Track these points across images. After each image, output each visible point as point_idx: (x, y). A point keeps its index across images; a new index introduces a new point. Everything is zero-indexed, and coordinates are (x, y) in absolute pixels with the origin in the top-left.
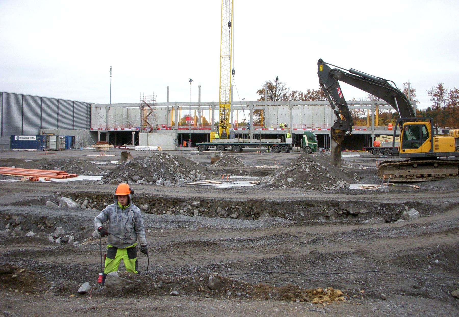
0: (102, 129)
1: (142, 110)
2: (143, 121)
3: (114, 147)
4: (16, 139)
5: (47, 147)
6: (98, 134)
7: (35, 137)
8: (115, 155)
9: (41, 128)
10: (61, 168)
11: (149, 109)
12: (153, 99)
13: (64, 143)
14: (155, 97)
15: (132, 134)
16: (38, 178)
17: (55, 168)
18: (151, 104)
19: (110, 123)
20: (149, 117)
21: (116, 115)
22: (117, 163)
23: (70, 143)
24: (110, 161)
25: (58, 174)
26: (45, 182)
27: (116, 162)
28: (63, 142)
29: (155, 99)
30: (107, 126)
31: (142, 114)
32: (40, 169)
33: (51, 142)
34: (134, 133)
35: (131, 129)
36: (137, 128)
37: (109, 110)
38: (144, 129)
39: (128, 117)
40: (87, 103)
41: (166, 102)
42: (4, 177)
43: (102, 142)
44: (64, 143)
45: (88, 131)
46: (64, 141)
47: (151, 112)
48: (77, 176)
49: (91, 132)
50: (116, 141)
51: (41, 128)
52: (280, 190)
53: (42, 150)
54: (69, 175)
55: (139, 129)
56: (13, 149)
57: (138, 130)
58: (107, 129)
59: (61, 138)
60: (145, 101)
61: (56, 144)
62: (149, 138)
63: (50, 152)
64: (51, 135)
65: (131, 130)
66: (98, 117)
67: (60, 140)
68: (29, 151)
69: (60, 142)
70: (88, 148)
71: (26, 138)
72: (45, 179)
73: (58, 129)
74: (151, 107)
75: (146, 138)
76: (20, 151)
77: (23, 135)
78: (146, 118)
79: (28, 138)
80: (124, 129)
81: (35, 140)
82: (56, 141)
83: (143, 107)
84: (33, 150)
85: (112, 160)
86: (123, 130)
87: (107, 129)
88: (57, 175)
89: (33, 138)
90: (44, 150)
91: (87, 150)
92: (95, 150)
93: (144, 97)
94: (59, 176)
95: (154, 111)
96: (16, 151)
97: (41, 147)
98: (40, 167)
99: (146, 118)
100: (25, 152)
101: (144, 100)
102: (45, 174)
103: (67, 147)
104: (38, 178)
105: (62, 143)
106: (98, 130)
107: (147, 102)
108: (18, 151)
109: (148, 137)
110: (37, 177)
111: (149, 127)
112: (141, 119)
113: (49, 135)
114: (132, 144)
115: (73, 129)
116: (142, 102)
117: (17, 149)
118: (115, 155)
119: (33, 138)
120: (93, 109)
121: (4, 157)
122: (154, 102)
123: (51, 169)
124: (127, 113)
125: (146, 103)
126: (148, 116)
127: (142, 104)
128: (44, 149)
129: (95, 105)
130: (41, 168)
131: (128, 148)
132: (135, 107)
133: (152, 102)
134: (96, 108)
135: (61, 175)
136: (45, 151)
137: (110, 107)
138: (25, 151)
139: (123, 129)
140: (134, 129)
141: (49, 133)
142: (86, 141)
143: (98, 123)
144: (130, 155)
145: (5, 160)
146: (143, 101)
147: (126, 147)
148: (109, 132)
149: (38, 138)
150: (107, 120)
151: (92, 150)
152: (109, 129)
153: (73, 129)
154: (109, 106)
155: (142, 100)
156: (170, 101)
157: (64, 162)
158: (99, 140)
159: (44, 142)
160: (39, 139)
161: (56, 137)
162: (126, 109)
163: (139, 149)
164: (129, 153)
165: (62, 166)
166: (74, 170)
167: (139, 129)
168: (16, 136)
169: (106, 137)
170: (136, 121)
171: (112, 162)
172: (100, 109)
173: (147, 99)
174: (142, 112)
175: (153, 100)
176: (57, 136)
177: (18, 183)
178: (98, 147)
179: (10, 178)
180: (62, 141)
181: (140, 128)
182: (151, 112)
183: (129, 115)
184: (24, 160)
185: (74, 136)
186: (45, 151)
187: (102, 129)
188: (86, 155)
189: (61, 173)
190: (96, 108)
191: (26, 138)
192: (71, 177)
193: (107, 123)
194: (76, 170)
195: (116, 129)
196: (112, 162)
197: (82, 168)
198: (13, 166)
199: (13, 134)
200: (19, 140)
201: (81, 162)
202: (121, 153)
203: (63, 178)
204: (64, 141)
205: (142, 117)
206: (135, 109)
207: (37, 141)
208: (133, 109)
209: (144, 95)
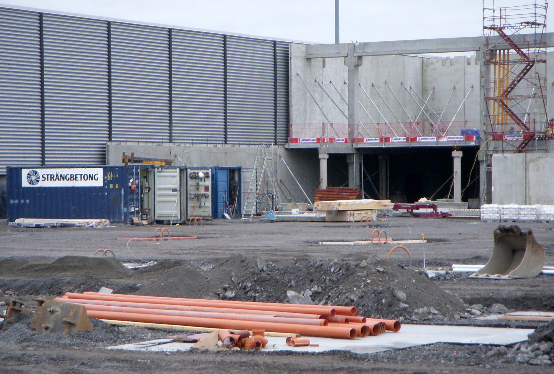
0: (332, 140)
1: (487, 63)
2: (495, 109)
3: (396, 208)
4: (25, 183)
5: (143, 212)
6: (318, 161)
7: (99, 172)
8: (429, 241)
9: (110, 139)
10: (309, 293)
11: (519, 57)
12: (532, 20)
13: (206, 196)
14: (541, 11)
15: (451, 159)
16: (262, 334)
17: (290, 293)
18: (526, 41)
19: (361, 118)
20: (513, 93)
21: (382, 85)
22: (481, 271)
23: (223, 196)
24: (446, 263)
25: (327, 318)
26: (289, 353)
27: (474, 268)
28: (202, 191)
29: (540, 20)
30: (351, 126)
31: (487, 81)
32: (224, 298)
33: (157, 192)
34: (457, 156)
35: (444, 140)
36: (467, 135)
37: (357, 66)
38: (498, 137)
39: (424, 91)
40: (275, 43)
41: (333, 42)
42: (112, 332)
43: (337, 189)
44: (206, 196)
45: (280, 150)
46: (207, 189)
47: (526, 71)
48: (396, 327)
49: (287, 149)
50: (383, 184)
51: (110, 139)
52: (149, 358)
53: (125, 222)
54: (371, 322)
55: (478, 138)
56: (18, 221)
57: (473, 144)
58: (353, 141)
59: (195, 177)
60: (500, 29)
61: (177, 199)
62: (532, 174)
63: (157, 229)
64: (157, 164)
65: (445, 141)
66: (317, 96)
67: (191, 182)
68: (80, 228)
69: (192, 190)
70: (295, 212)
71: (63, 178)
72: (288, 340)
73: (171, 141)
74: (524, 50)
75: (520, 173)
76: (44, 227)
77: (43, 165)
78: (507, 93)
79: (73, 178)
80: (418, 139)
81: (99, 183)
82: (177, 186)
83: (492, 53)
84: (93, 222)
85: (457, 261)
86: (413, 145)
87: (353, 141)
88: (325, 324)
89: (91, 177)
90: (132, 223)
91: (295, 220)
92: (323, 220)
93: (497, 13)
94: (331, 327)
95: (538, 67)
96: (28, 227)
97: (124, 210)
98: (225, 289)
99: (507, 93)
100: (65, 232)
101: (497, 23)
102: (271, 317)
103: (216, 214)
104: (262, 334)
105: (198, 197)
106: (317, 146)
107: (507, 32)
108: (38, 226)
109: (526, 169)
110: (259, 331)
111: (517, 127)
112: (487, 99)
113: (153, 167)
114: (451, 197)
115: (226, 143)
116: (487, 32)
117: (33, 222)
118: (429, 241)
119: (91, 177)
120: (296, 65)
121: (40, 254)
122: (539, 30)
123: (268, 299)
124: (419, 78)
125: (503, 35)
126: (513, 86)
127: (488, 39)
128: (136, 220)
129: (303, 48)
130: (230, 294)
131: (445, 210)
132: (452, 55)
133: (530, 30)
134: (309, 59)
135: (336, 322)
136: (138, 225)
137: (360, 57)
138: (64, 226)
139: (387, 140)
140: (458, 139)
141: (148, 160)
142: (275, 190)
143: (318, 120)
144: (534, 242)
145: (50, 262)
146: (493, 28)
147: (440, 210)
148: (358, 150)
149: (110, 176)
150: (351, 106)
151: (312, 220)
152: (361, 140)
153: (226, 143)
154: (359, 52)
155: (489, 24)
156: (341, 41)
157: (322, 269)
158: (324, 185)
159: (132, 192)
160: (114, 181)
161: (178, 170)
162: (418, 65)
163: (496, 216)
164: (530, 233)
165: (315, 288)
166: (369, 302)
167: (478, 138)
168: (25, 172)
169: (347, 171)
170: (456, 107)
171: (458, 268)
172: (324, 66)
173: (510, 21)
174: (488, 70)
175: (533, 24)
176: (183, 170)
177: (186, 358)
178: (336, 208)
179: (134, 337)
180: (198, 187)
181: (482, 135)
182: (526, 71)
183: (429, 86)
184: (118, 261)
185: (239, 169)
186: (138, 225)
187: (332, 140)
188: (317, 242)
189: (337, 317)
190: (309, 59)
191: (63, 178)
192: (377, 330)
193: (351, 116)
194: (379, 302)
195: (387, 140)
196: (458, 268)
197: (401, 295)
198: (103, 288)
199: (14, 164)
200: (38, 185)
201: (389, 269)
202: (496, 235)
203: (353, 334)
204: (207, 189)
205: (488, 90)
206: (452, 62)
207: (109, 190)
208: (444, 61)
209: (498, 5)
